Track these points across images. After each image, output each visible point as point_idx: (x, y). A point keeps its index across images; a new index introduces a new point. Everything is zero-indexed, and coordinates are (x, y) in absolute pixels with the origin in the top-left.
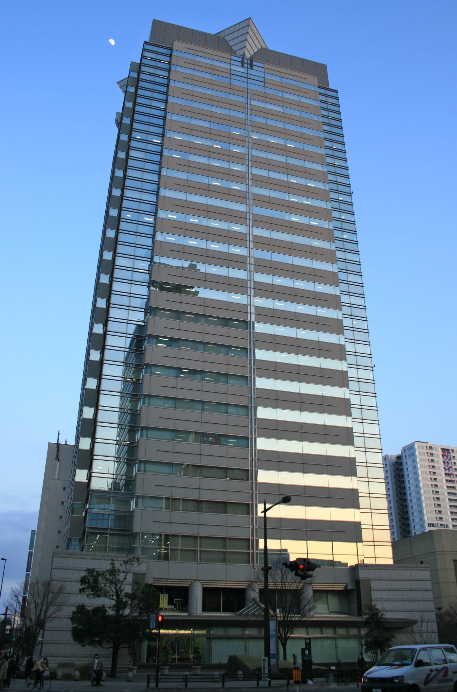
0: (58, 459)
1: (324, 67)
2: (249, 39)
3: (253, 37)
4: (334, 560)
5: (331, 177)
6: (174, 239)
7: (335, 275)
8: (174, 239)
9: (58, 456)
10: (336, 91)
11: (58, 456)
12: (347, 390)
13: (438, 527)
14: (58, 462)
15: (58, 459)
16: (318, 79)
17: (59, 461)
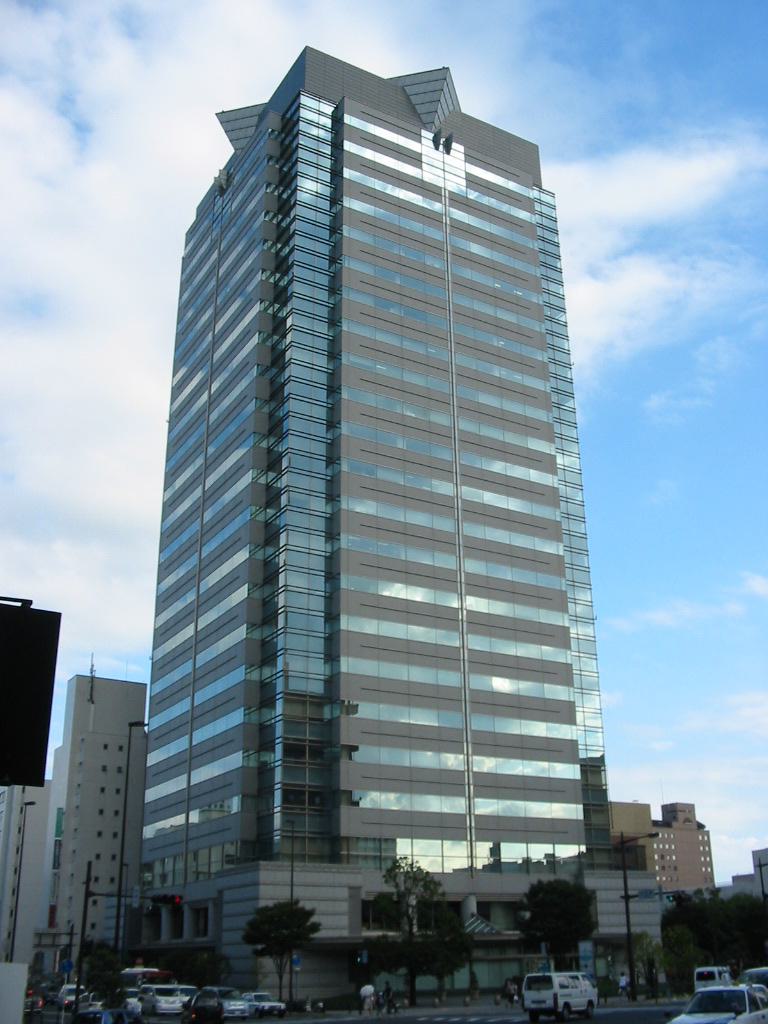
0: (91, 700)
1: (534, 149)
2: (442, 100)
3: (448, 96)
4: (557, 855)
5: (539, 232)
6: (156, 970)
7: (547, 396)
8: (156, 970)
9: (91, 697)
10: (553, 195)
11: (91, 697)
12: (553, 446)
13: (726, 984)
14: (92, 706)
15: (91, 700)
16: (604, 792)
17: (93, 703)
